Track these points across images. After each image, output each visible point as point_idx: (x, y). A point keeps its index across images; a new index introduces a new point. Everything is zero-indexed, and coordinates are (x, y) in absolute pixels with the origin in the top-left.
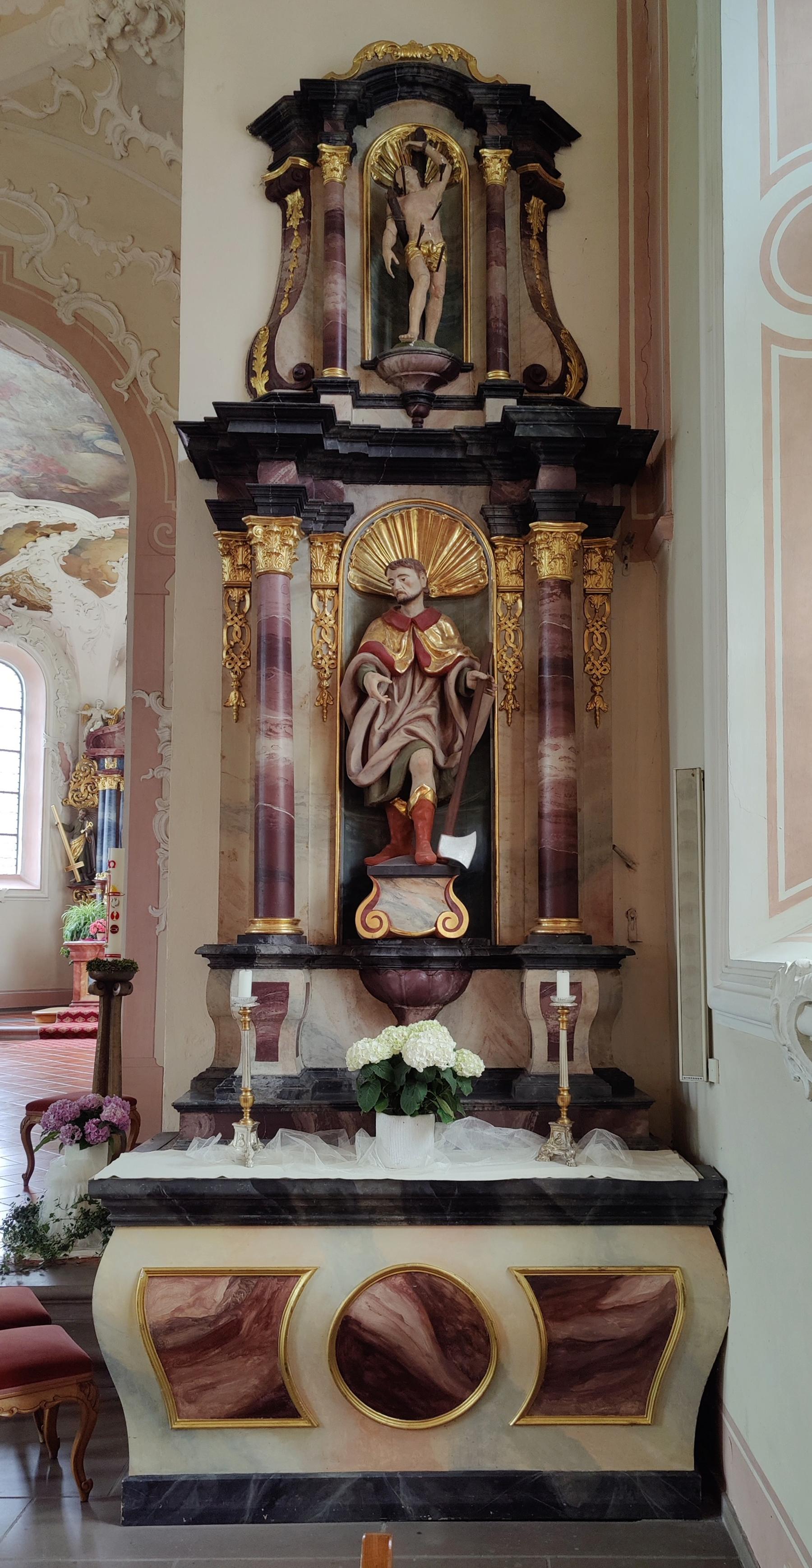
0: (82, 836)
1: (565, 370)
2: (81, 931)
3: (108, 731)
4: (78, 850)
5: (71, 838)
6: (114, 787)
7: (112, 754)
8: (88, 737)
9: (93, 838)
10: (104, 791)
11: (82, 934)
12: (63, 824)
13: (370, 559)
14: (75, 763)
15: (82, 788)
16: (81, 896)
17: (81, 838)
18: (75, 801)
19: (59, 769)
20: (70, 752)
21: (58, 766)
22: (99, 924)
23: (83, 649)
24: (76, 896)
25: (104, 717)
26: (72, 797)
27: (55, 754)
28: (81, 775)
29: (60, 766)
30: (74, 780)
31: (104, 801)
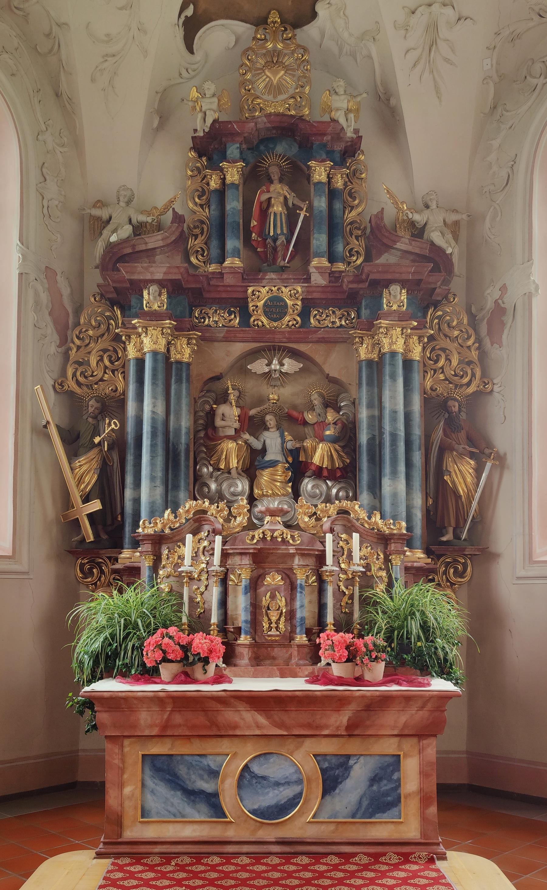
0: (95, 451)
2: (116, 654)
3: (143, 247)
4: (87, 479)
5: (72, 455)
6: (161, 347)
7: (159, 276)
8: (104, 257)
9: (115, 456)
10: (140, 363)
11: (119, 663)
12: (58, 427)
14: (78, 311)
15: (93, 361)
16: (91, 570)
17: (93, 453)
18: (79, 384)
19: (48, 319)
20: (69, 290)
21: (47, 313)
22: (166, 640)
23: (93, 80)
24: (82, 571)
25: (134, 221)
26: (74, 375)
27: (40, 289)
28: (91, 333)
29: (50, 314)
30: (78, 342)
31: (140, 381)
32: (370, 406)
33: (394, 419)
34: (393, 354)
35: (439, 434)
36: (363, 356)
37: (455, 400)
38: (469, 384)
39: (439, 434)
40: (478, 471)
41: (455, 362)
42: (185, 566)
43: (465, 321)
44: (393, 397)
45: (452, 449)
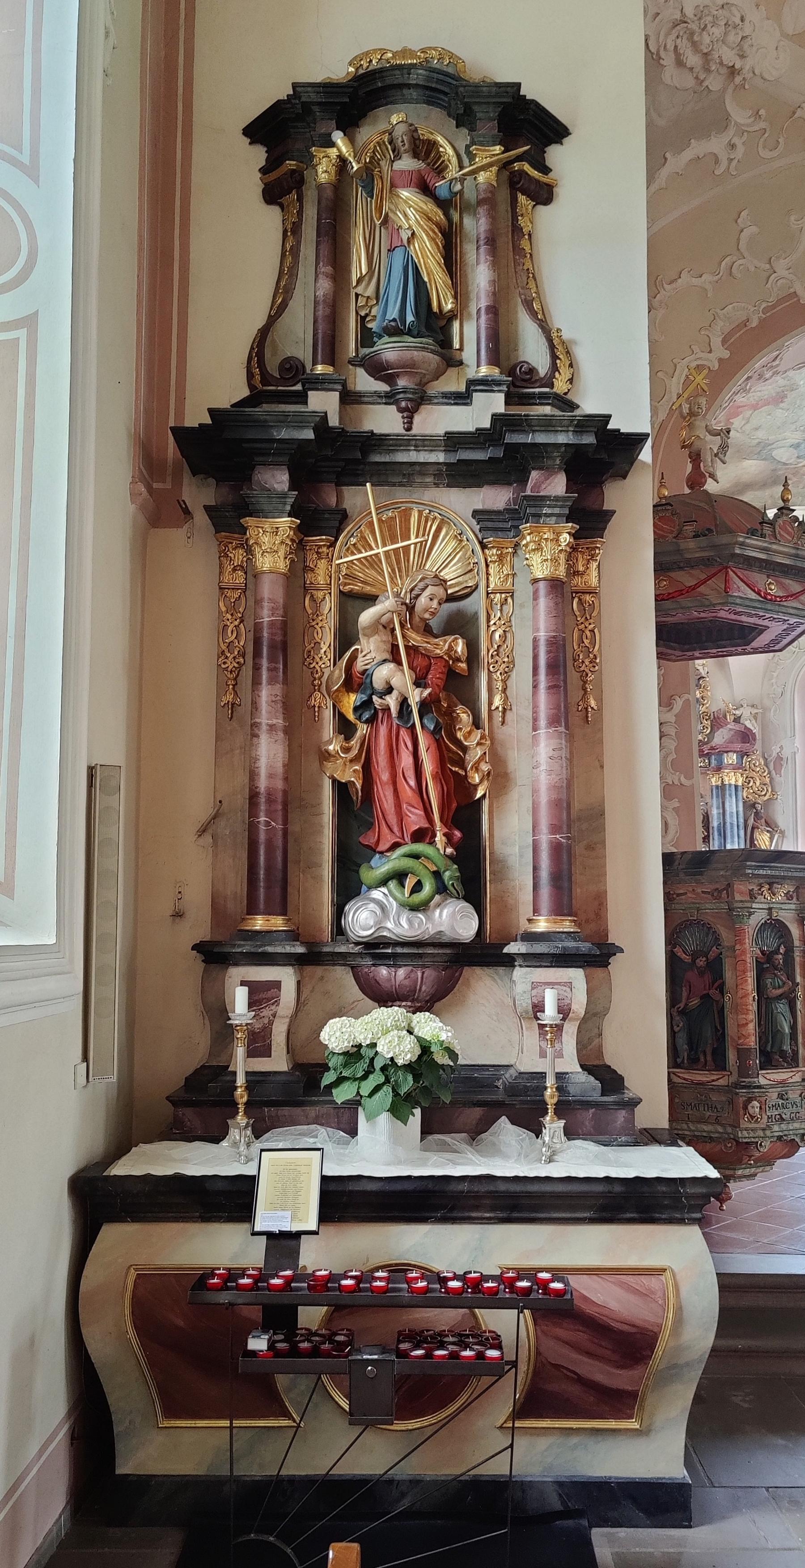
1: (554, 368)
13: (406, 1215)
32: (718, 808)
33: (731, 816)
34: (730, 785)
35: (751, 822)
36: (714, 784)
37: (759, 804)
38: (765, 795)
39: (751, 822)
40: (771, 839)
41: (758, 783)
42: (243, 983)
43: (763, 763)
44: (731, 806)
45: (758, 828)
